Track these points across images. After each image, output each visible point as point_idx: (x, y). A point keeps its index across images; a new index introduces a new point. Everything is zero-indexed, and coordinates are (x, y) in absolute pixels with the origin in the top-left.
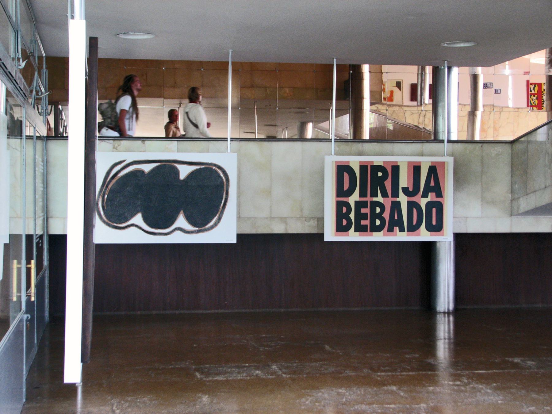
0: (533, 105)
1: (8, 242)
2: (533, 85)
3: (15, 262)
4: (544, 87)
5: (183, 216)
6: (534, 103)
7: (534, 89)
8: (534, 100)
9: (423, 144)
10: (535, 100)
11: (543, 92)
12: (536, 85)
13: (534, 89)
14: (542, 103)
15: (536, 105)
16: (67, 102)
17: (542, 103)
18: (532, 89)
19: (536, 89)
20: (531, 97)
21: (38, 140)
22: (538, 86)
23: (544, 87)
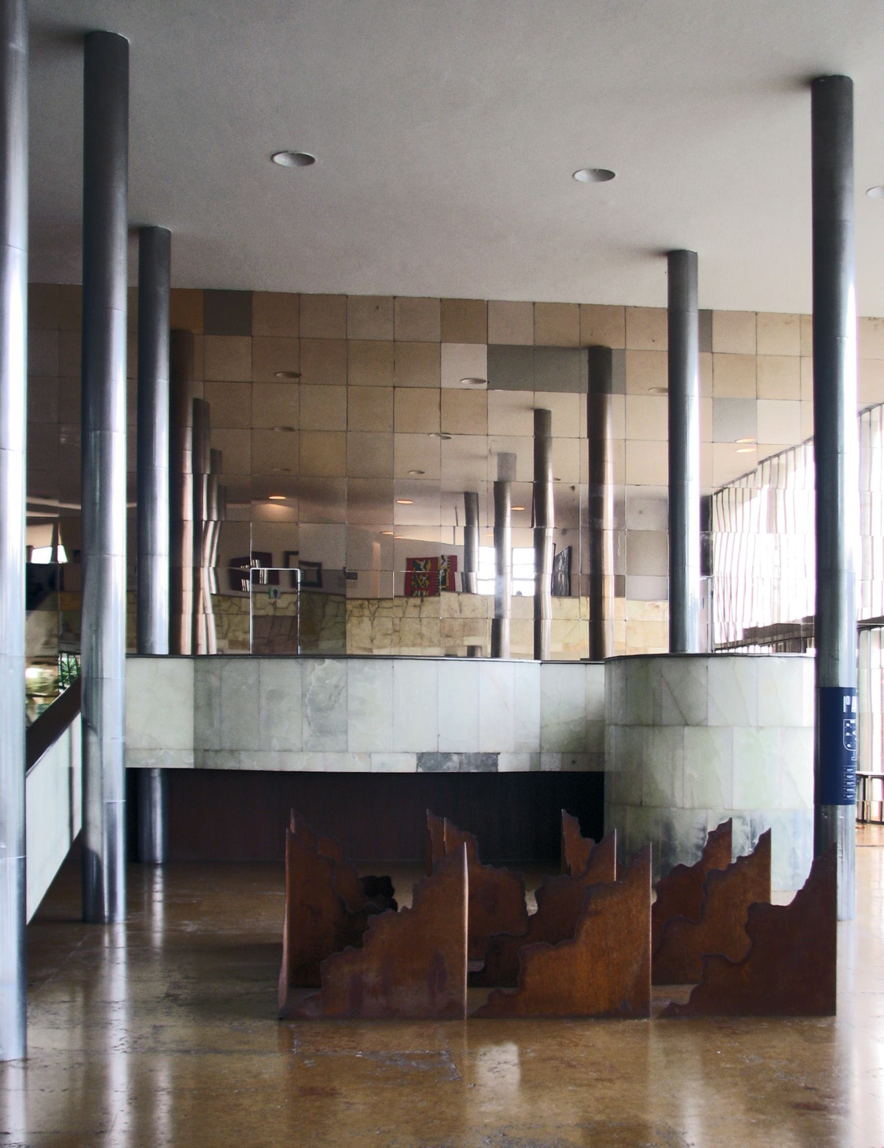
0: (423, 587)
1: (455, 573)
2: (424, 561)
3: (293, 832)
4: (60, 696)
5: (676, 839)
6: (423, 585)
7: (425, 567)
8: (423, 580)
9: (788, 620)
10: (424, 580)
11: (448, 568)
12: (429, 561)
13: (425, 567)
14: (437, 584)
15: (427, 586)
16: (823, 1023)
17: (437, 584)
18: (422, 567)
19: (429, 566)
20: (419, 578)
21: (295, 550)
22: (431, 561)
23: (60, 696)
